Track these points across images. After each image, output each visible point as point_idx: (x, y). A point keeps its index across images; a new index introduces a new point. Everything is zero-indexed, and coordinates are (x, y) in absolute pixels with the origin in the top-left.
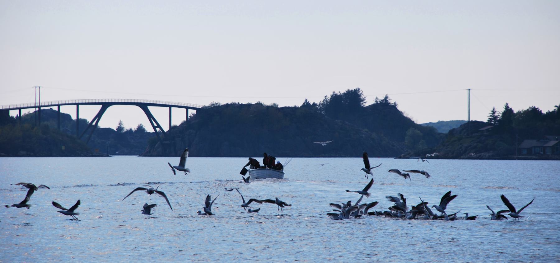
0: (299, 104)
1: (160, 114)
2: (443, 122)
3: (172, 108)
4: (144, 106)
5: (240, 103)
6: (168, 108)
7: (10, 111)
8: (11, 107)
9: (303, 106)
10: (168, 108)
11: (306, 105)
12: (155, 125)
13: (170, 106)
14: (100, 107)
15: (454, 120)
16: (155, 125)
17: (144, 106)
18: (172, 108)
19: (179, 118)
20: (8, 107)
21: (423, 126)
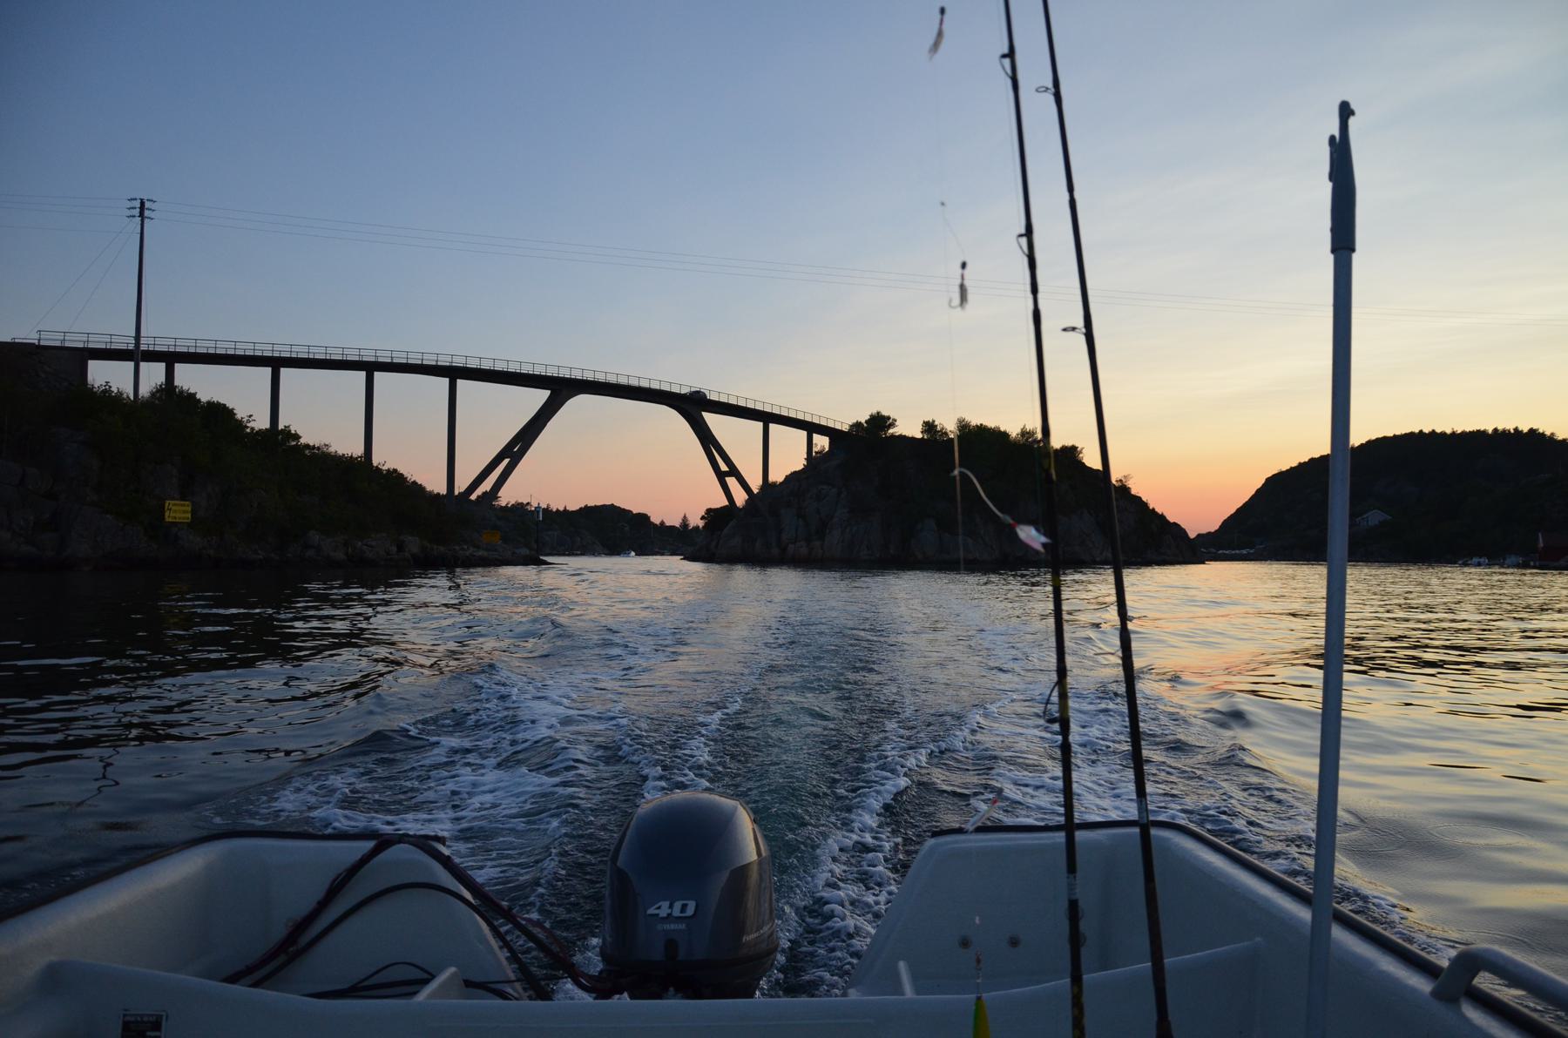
0: (1392, 435)
1: (737, 436)
2: (795, 472)
3: (379, 376)
4: (692, 406)
5: (1002, 429)
6: (267, 372)
7: (93, 365)
8: (97, 343)
9: (1451, 434)
10: (267, 372)
11: (1395, 435)
12: (724, 468)
13: (371, 368)
14: (541, 396)
15: (1398, 433)
16: (724, 468)
17: (692, 406)
18: (379, 376)
19: (790, 454)
20: (75, 341)
21: (491, 995)
